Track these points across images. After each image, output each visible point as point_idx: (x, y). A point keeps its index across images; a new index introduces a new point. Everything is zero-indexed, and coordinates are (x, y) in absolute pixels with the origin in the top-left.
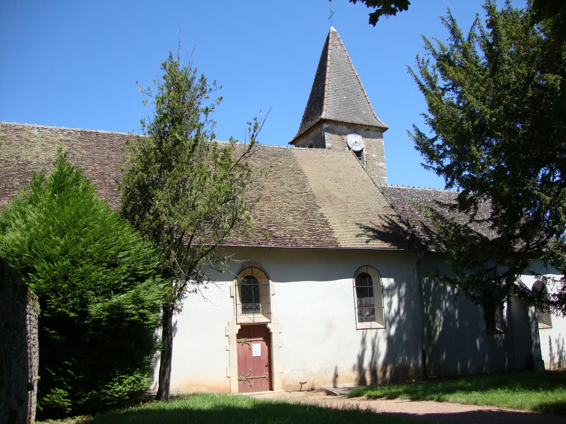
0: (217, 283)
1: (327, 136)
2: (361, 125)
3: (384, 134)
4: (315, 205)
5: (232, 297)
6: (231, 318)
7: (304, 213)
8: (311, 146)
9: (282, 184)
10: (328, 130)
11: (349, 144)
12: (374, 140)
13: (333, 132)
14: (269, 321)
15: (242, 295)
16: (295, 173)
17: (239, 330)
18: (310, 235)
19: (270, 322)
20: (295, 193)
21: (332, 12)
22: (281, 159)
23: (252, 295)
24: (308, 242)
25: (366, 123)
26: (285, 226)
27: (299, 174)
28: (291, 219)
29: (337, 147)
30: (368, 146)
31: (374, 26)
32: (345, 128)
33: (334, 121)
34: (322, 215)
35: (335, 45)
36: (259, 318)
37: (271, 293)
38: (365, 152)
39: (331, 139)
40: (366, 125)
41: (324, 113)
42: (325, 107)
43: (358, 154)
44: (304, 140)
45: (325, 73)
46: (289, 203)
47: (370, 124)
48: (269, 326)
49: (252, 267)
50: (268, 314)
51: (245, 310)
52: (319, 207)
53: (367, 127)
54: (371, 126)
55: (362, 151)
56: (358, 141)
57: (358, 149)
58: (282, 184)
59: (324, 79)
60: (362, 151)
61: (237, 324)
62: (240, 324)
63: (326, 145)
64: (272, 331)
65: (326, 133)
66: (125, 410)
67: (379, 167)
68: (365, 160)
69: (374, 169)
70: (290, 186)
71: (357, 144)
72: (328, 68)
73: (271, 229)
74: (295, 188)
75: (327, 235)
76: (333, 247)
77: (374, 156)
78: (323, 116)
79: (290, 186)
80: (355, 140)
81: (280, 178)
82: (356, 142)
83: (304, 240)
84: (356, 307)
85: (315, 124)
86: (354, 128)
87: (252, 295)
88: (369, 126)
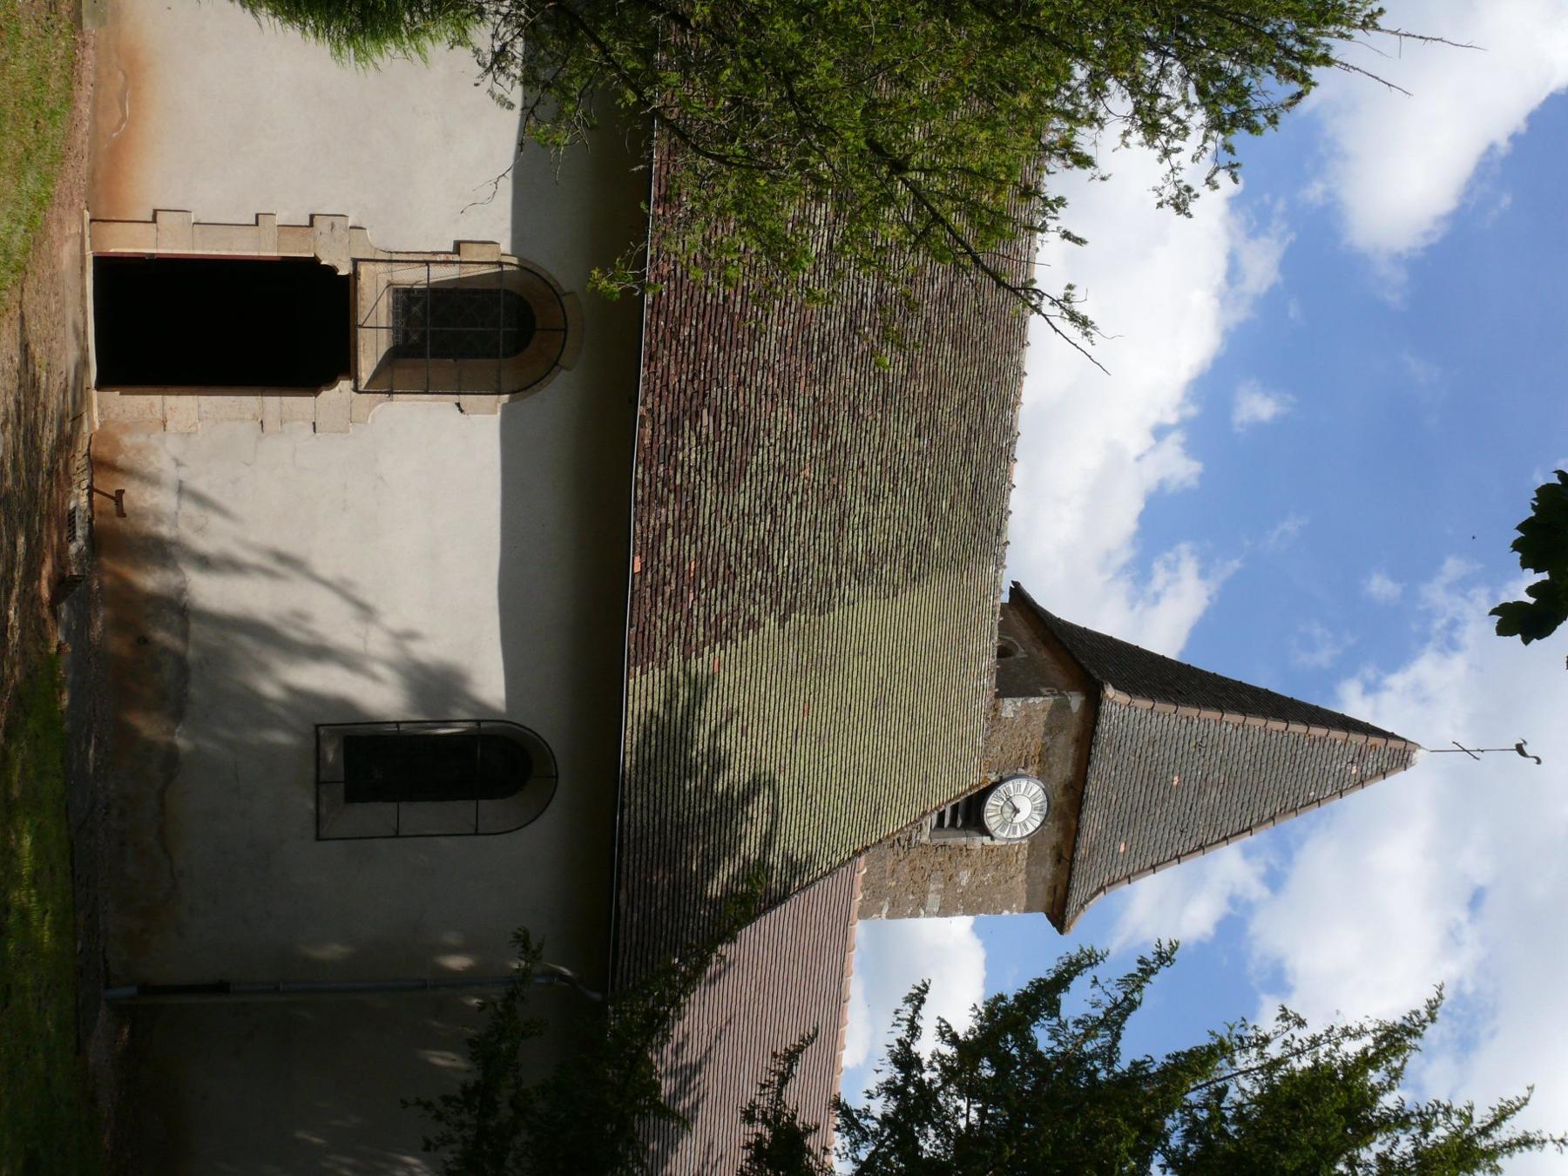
0: (507, 185)
1: (1040, 703)
2: (1078, 831)
3: (1040, 920)
4: (791, 608)
5: (458, 246)
6: (378, 239)
7: (762, 557)
8: (1003, 653)
9: (875, 498)
10: (1061, 708)
11: (1010, 784)
12: (1021, 877)
13: (1051, 729)
14: (362, 388)
15: (463, 292)
16: (909, 554)
17: (331, 270)
18: (678, 564)
19: (356, 389)
20: (838, 539)
21: (1477, 754)
22: (962, 510)
23: (462, 332)
24: (652, 551)
25: (1082, 852)
26: (715, 475)
27: (908, 567)
28: (743, 501)
29: (999, 738)
30: (1001, 856)
31: (1419, 746)
32: (1063, 770)
33: (1094, 732)
34: (754, 624)
35: (1361, 755)
36: (371, 347)
37: (466, 400)
38: (979, 841)
39: (1028, 718)
40: (1074, 849)
41: (1123, 698)
42: (1143, 704)
43: (969, 813)
44: (1025, 633)
45: (1265, 716)
46: (800, 506)
47: (1077, 866)
48: (345, 385)
49: (566, 331)
50: (389, 380)
51: (406, 300)
52: (783, 620)
53: (1066, 855)
54: (1071, 870)
55: (985, 831)
56: (1019, 818)
57: (992, 818)
58: (875, 498)
59: (1244, 710)
60: (985, 831)
61: (355, 262)
62: (355, 274)
63: (1008, 701)
64: (325, 394)
65: (1051, 699)
66: (45, 458)
67: (925, 893)
68: (950, 841)
69: (917, 877)
70: (865, 526)
71: (1008, 811)
72: (1281, 726)
73: (706, 419)
74: (856, 543)
75: (674, 628)
76: (629, 645)
77: (964, 877)
78: (1110, 691)
79: (865, 526)
80: (1022, 807)
81: (894, 491)
82: (1016, 811)
83: (662, 537)
84: (402, 727)
85: (1081, 666)
86: (1068, 808)
87: (462, 332)
88: (1072, 860)
